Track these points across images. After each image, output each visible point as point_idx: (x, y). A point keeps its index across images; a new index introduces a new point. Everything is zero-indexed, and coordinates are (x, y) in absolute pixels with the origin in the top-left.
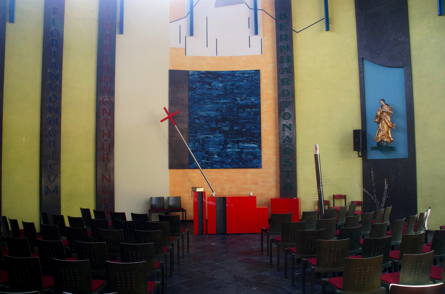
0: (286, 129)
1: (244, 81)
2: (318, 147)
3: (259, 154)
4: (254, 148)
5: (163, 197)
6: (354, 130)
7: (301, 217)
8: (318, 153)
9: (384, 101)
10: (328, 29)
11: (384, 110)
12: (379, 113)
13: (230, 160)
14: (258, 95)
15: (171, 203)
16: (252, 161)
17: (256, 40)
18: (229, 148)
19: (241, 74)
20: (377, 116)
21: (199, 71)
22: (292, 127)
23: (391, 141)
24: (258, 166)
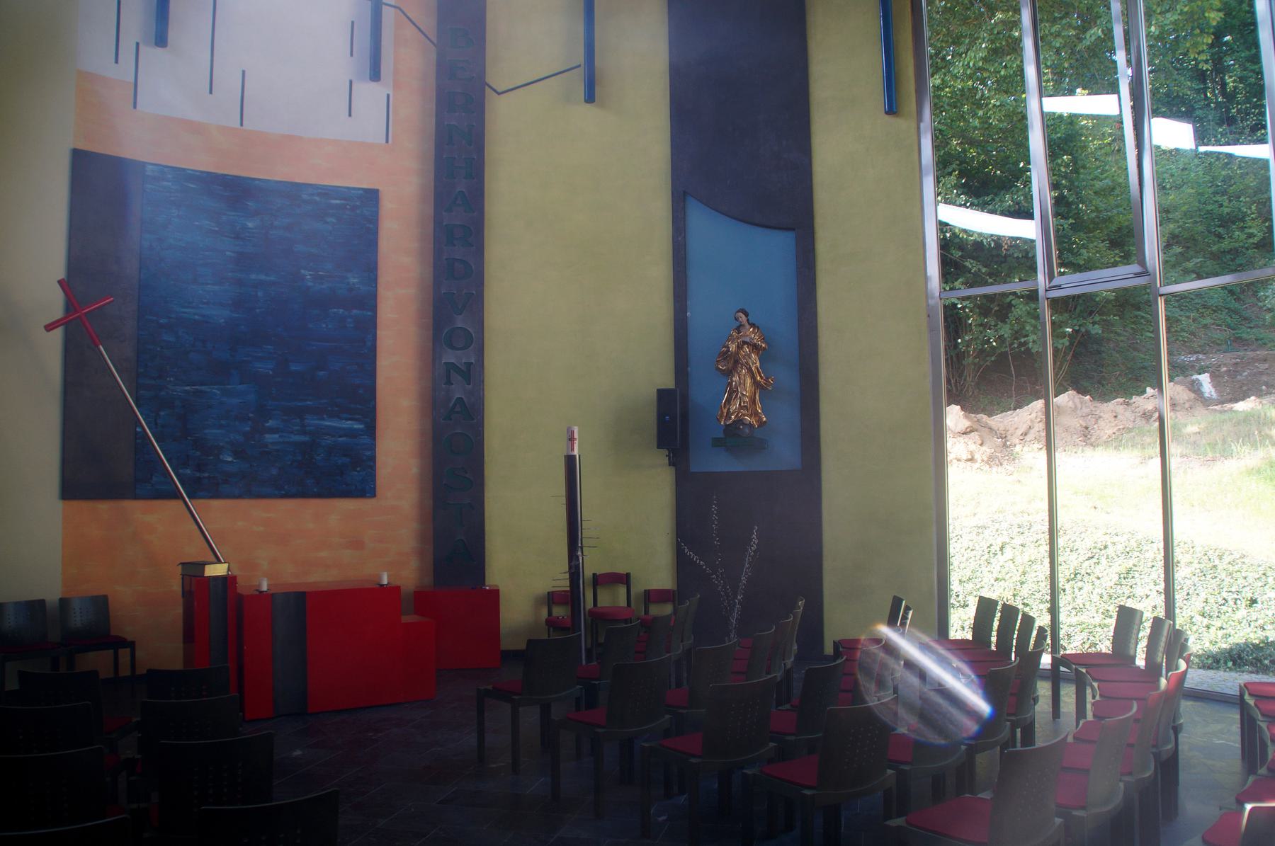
0: (456, 377)
1: (329, 220)
2: (576, 436)
3: (368, 453)
4: (352, 433)
5: (43, 601)
6: (658, 390)
7: (829, 649)
8: (576, 452)
9: (746, 314)
10: (590, 98)
11: (747, 339)
12: (733, 347)
13: (274, 472)
14: (371, 271)
15: (78, 619)
16: (347, 473)
17: (372, 96)
18: (273, 431)
19: (319, 194)
20: (725, 355)
21: (179, 169)
22: (473, 373)
23: (762, 424)
24: (365, 489)
